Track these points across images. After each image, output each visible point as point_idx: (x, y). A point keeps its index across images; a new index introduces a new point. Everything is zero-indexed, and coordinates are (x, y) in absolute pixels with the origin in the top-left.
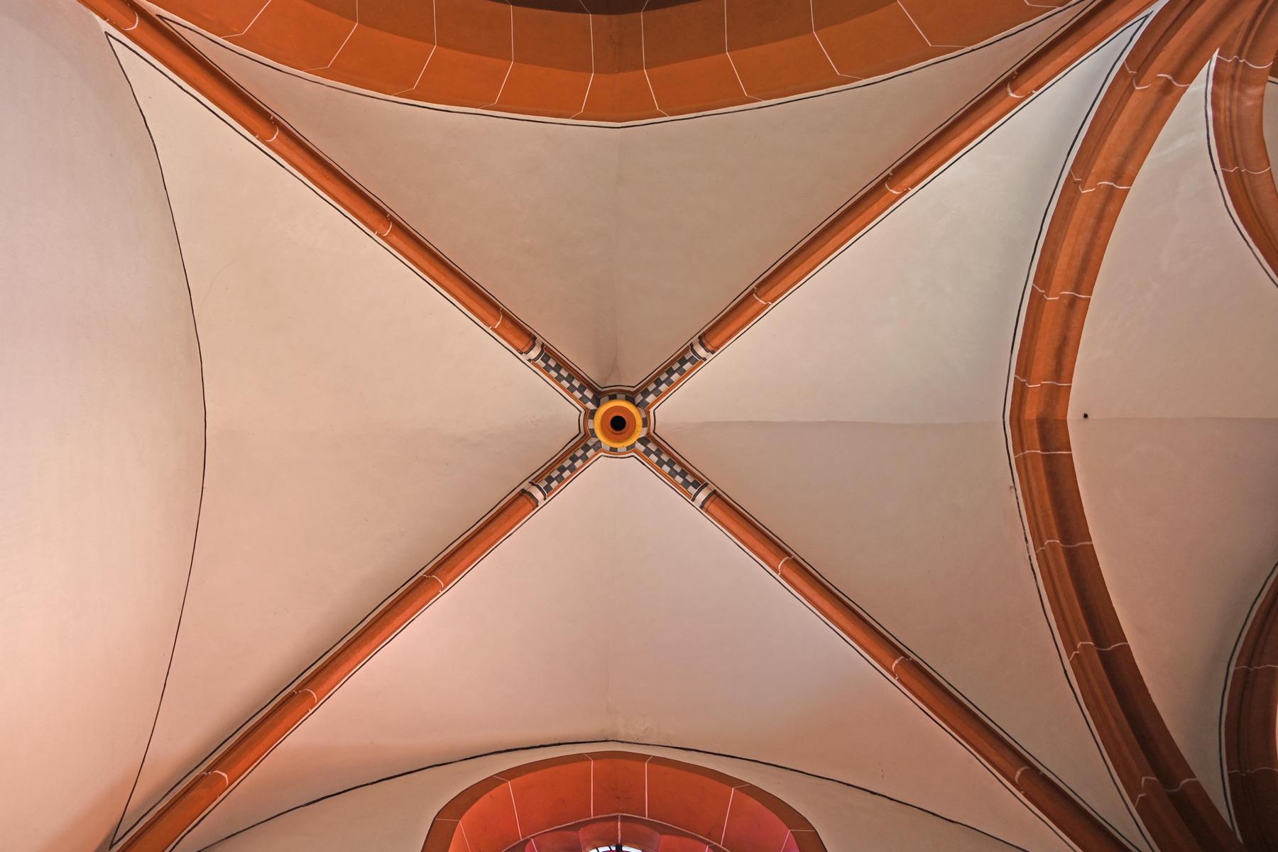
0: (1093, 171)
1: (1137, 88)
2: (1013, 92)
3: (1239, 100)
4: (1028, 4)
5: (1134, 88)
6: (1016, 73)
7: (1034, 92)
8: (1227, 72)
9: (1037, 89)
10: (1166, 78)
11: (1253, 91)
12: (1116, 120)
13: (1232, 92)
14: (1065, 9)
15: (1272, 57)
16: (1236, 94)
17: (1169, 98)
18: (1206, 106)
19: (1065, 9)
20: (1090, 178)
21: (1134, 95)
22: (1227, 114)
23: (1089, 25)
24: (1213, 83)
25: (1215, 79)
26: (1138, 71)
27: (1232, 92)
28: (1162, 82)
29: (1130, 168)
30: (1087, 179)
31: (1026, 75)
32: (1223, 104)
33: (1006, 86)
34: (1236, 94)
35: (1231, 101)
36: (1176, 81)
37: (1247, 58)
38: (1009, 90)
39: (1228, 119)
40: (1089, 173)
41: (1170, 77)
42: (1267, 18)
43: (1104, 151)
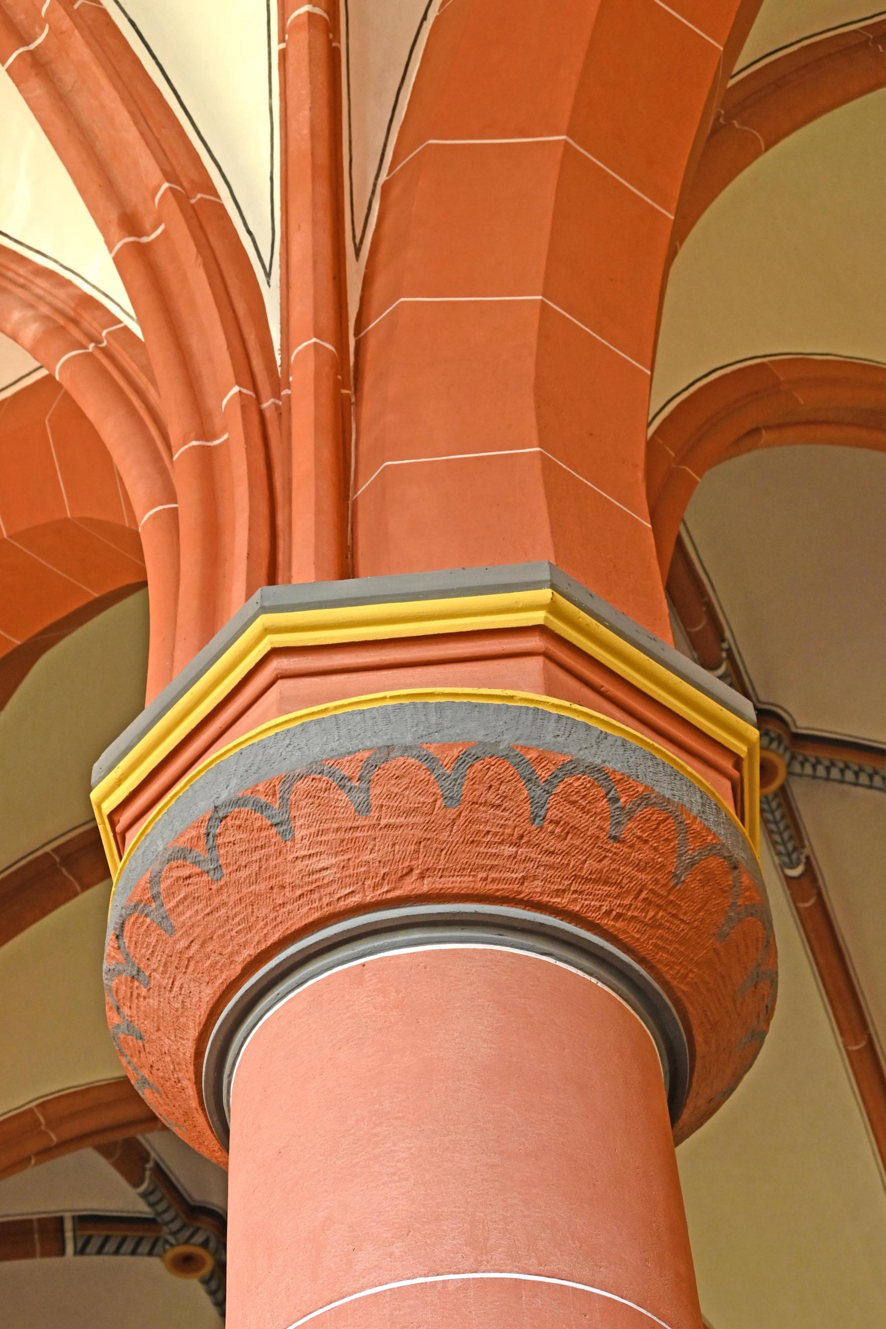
0: (76, 33)
1: (166, 185)
2: (310, 14)
3: (32, 306)
4: (431, 142)
5: (168, 181)
6: (334, 44)
7: (283, 46)
8: (88, 319)
9: (283, 54)
10: (148, 235)
11: (31, 331)
12: (136, 124)
13: (50, 305)
14: (375, 185)
15: (67, 384)
16: (45, 310)
17: (114, 216)
18: (56, 262)
19: (375, 185)
20: (68, 20)
21: (159, 175)
22: (22, 281)
23: (324, 192)
24: (115, 246)
25: (91, 299)
26: (192, 206)
27: (50, 305)
28: (148, 226)
29: (39, 89)
30: (69, 15)
31: (321, 52)
32: (42, 285)
33: (328, 13)
34: (45, 310)
35: (40, 298)
36: (133, 243)
37: (90, 355)
38: (318, 11)
39: (10, 274)
40: (77, 26)
41: (145, 240)
42: (132, 412)
43: (97, 72)
